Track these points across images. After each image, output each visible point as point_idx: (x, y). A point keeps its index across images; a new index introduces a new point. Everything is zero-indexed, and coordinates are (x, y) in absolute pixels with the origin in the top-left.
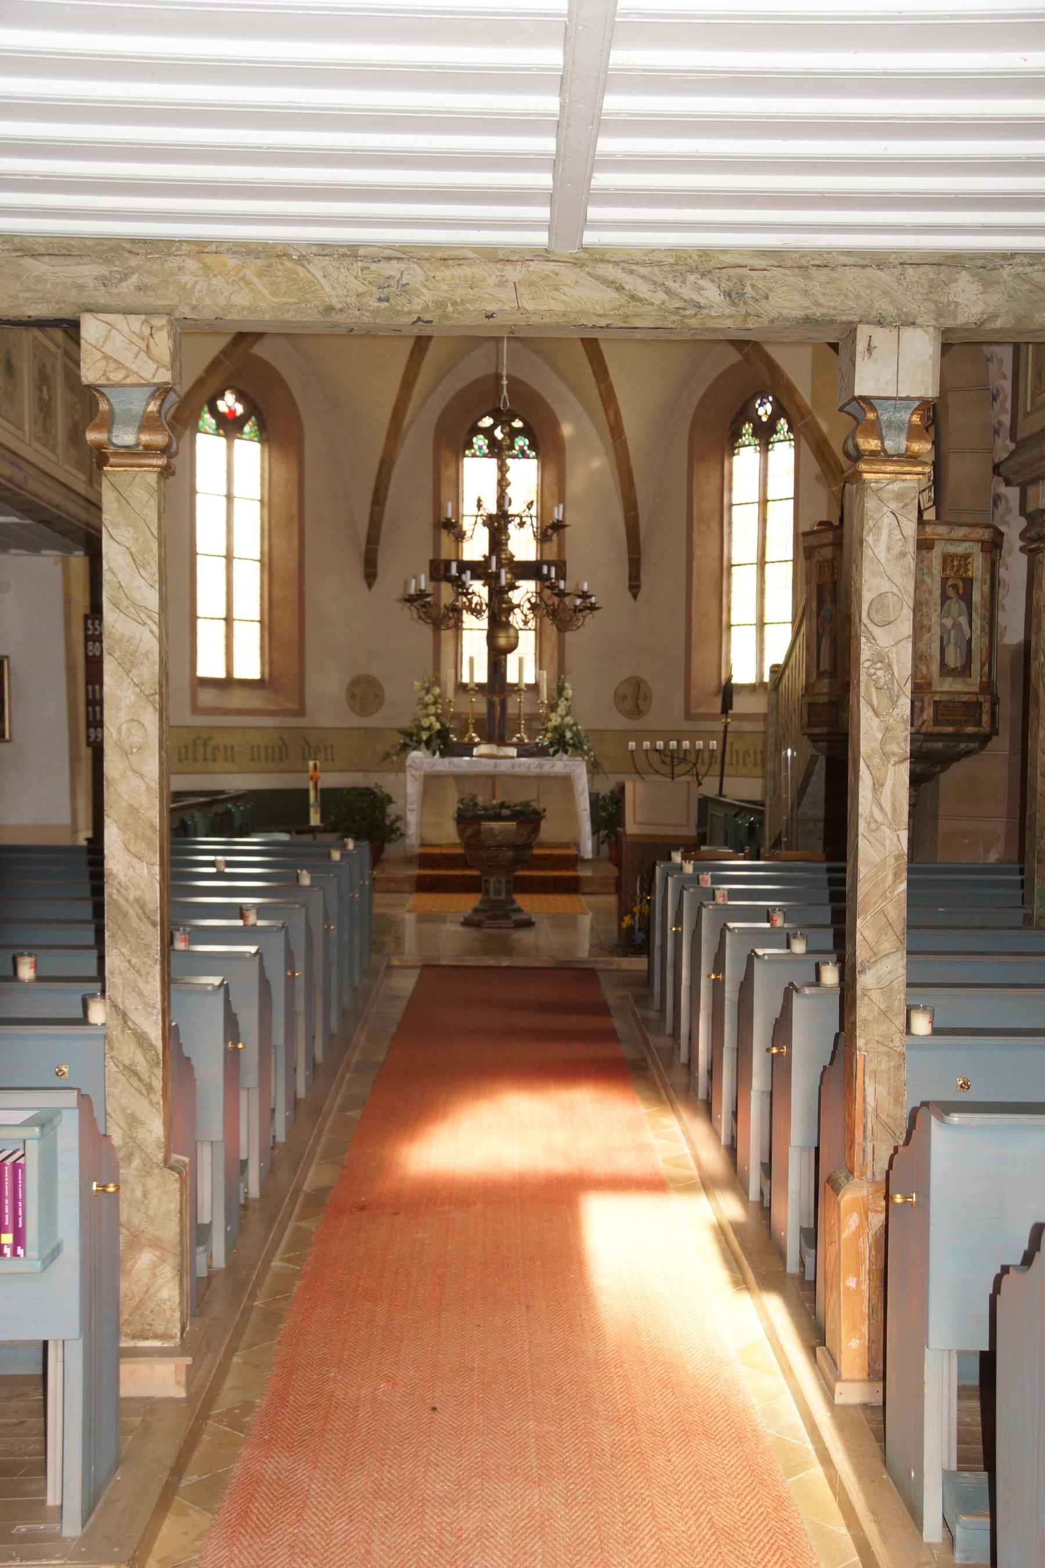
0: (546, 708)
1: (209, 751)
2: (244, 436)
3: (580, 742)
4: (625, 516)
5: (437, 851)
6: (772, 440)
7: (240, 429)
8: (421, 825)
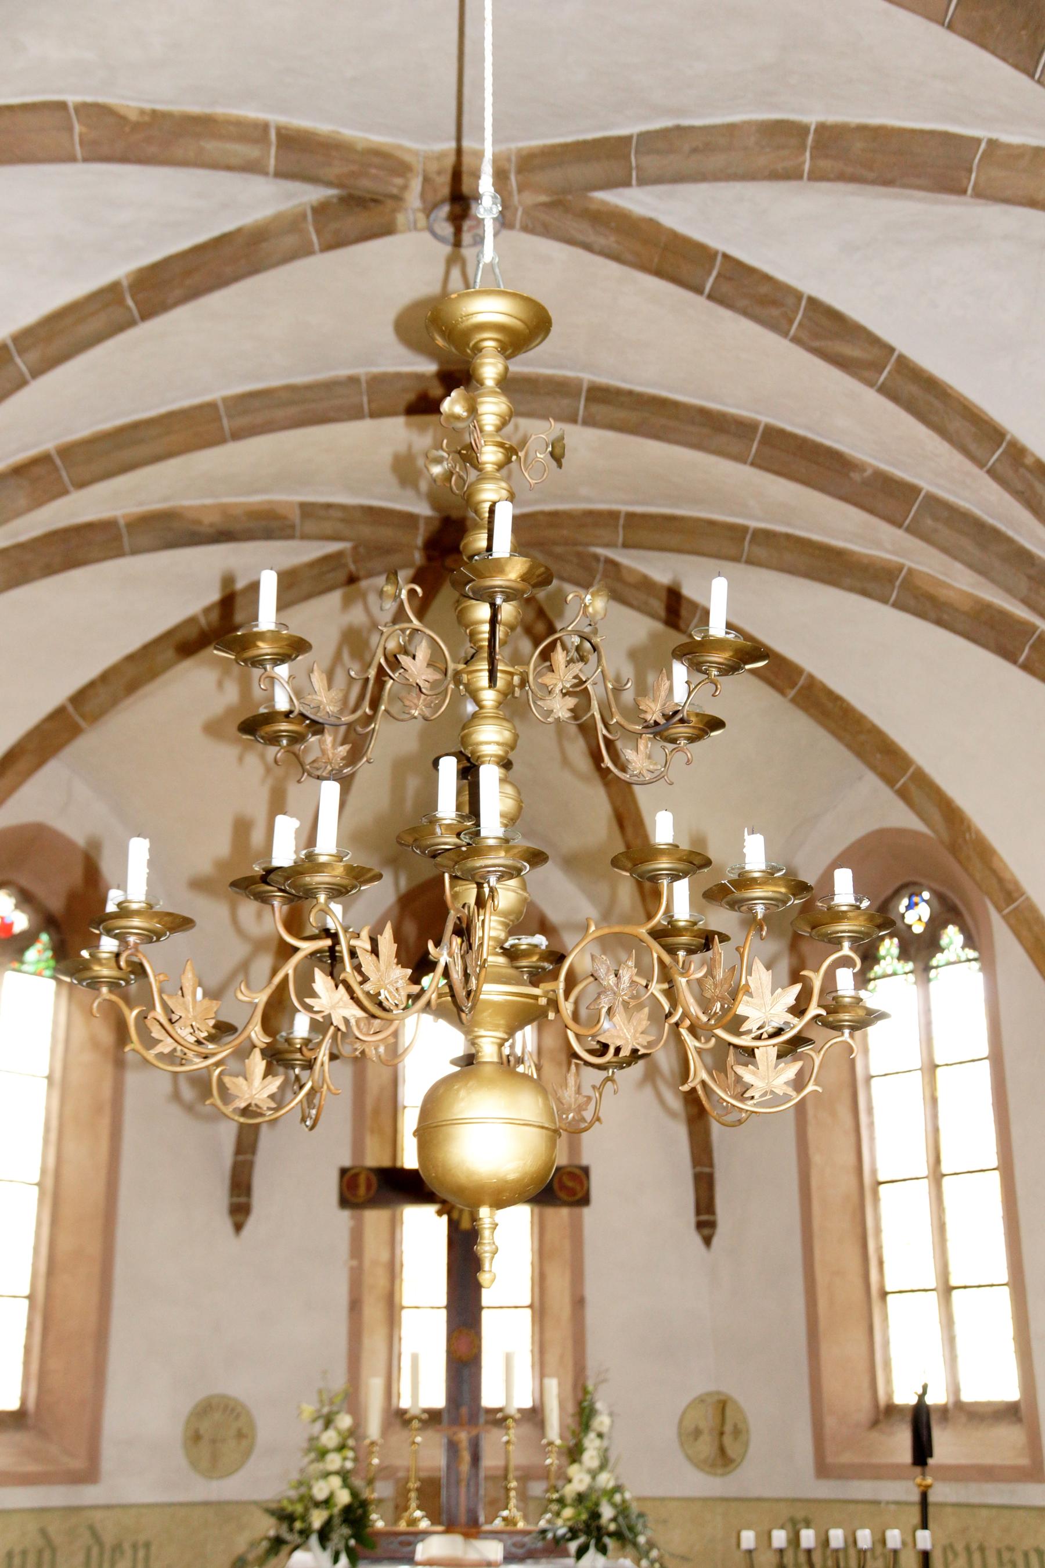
0: (560, 1453)
2: (25, 968)
3: (631, 1529)
6: (934, 962)
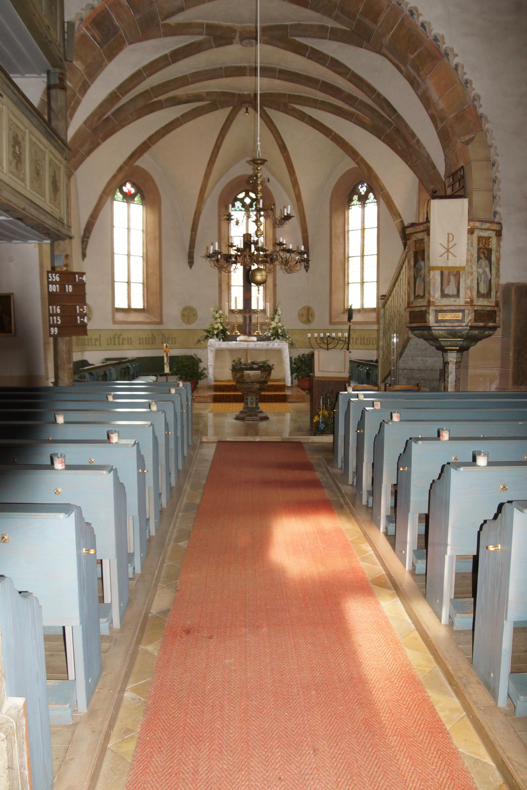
1: (121, 341)
3: (285, 334)
4: (302, 236)
5: (222, 383)
6: (366, 202)
7: (134, 198)
8: (214, 373)
